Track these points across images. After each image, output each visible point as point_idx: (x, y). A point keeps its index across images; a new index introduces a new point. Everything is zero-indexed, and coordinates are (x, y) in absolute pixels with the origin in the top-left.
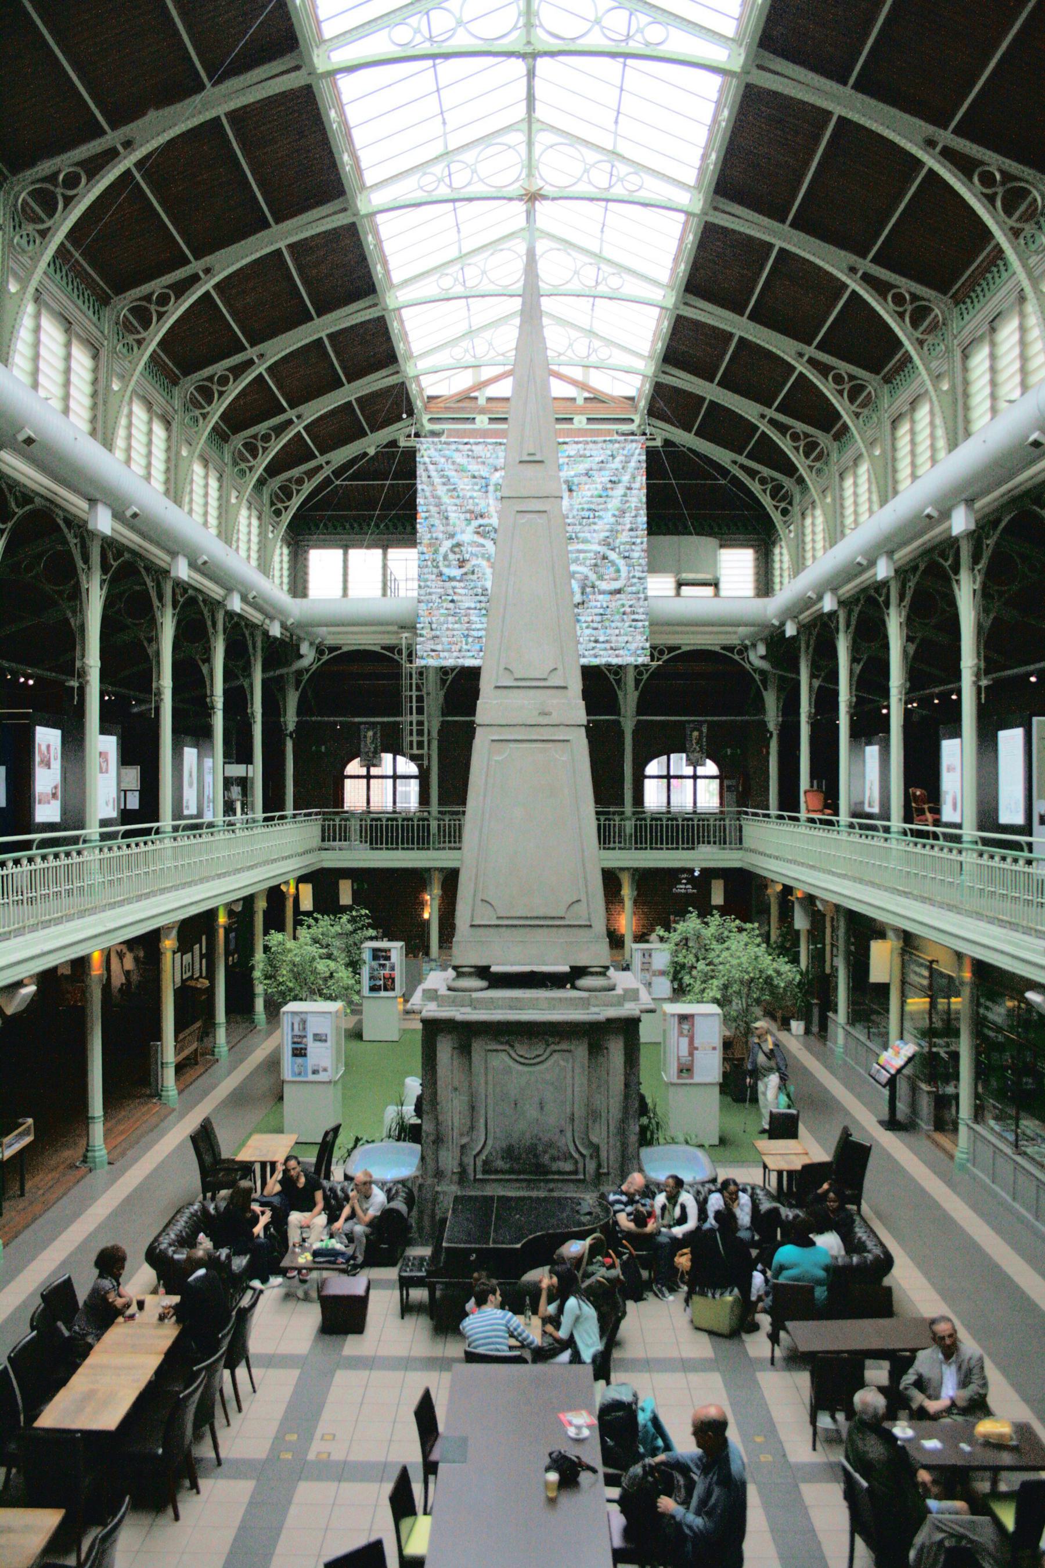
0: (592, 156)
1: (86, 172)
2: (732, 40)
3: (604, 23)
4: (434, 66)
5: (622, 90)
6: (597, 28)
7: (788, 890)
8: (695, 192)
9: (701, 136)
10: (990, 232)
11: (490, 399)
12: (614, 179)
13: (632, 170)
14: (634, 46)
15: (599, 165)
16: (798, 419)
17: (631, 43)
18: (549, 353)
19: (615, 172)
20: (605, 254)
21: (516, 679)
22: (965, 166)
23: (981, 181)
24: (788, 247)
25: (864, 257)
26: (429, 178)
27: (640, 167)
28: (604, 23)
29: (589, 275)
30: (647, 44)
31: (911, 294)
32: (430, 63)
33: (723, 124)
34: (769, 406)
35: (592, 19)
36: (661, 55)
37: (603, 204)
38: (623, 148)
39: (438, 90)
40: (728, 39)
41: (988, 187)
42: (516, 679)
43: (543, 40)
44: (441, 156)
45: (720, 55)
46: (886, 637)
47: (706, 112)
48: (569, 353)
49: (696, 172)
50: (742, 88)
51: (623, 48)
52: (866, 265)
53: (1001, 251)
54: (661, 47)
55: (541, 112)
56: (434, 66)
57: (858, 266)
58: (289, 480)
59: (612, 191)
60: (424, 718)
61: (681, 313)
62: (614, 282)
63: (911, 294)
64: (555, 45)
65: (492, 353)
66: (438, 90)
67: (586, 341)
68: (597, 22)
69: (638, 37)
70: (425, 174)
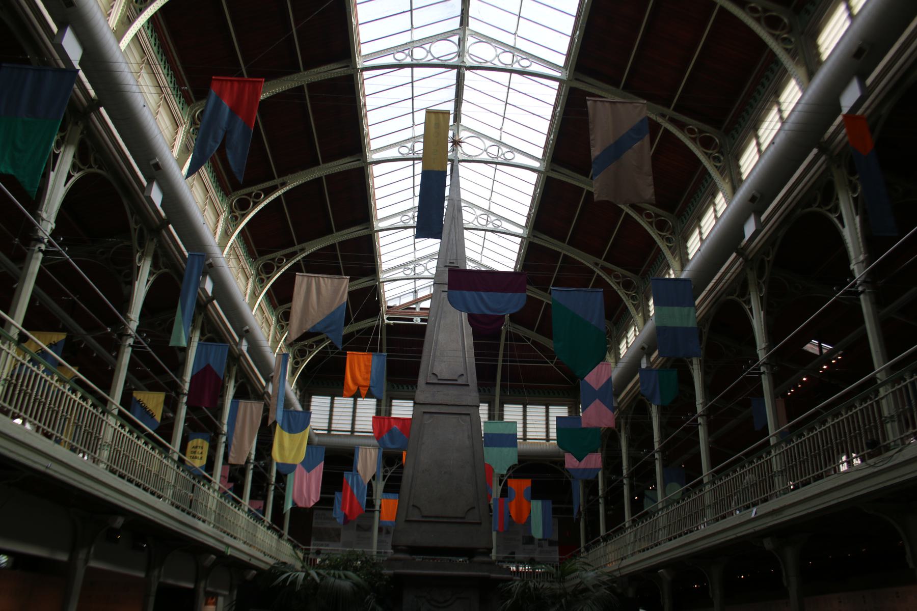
0: (479, 212)
1: (263, 192)
2: (562, 67)
3: (488, 151)
4: (413, 165)
5: (509, 88)
6: (485, 152)
8: (525, 229)
10: (655, 241)
11: (421, 309)
13: (496, 218)
14: (500, 160)
16: (618, 265)
17: (499, 159)
18: (464, 222)
20: (517, 46)
23: (614, 277)
24: (567, 253)
25: (669, 107)
26: (404, 218)
28: (488, 151)
30: (506, 159)
31: (655, 214)
32: (413, 280)
40: (561, 67)
41: (692, 134)
43: (469, 61)
44: (411, 138)
45: (536, 165)
46: (656, 479)
48: (475, 222)
49: (530, 198)
50: (545, 178)
52: (601, 262)
53: (660, 250)
54: (527, 69)
56: (413, 165)
57: (598, 262)
58: (273, 259)
62: (525, 63)
63: (655, 214)
64: (466, 158)
65: (430, 57)
68: (486, 150)
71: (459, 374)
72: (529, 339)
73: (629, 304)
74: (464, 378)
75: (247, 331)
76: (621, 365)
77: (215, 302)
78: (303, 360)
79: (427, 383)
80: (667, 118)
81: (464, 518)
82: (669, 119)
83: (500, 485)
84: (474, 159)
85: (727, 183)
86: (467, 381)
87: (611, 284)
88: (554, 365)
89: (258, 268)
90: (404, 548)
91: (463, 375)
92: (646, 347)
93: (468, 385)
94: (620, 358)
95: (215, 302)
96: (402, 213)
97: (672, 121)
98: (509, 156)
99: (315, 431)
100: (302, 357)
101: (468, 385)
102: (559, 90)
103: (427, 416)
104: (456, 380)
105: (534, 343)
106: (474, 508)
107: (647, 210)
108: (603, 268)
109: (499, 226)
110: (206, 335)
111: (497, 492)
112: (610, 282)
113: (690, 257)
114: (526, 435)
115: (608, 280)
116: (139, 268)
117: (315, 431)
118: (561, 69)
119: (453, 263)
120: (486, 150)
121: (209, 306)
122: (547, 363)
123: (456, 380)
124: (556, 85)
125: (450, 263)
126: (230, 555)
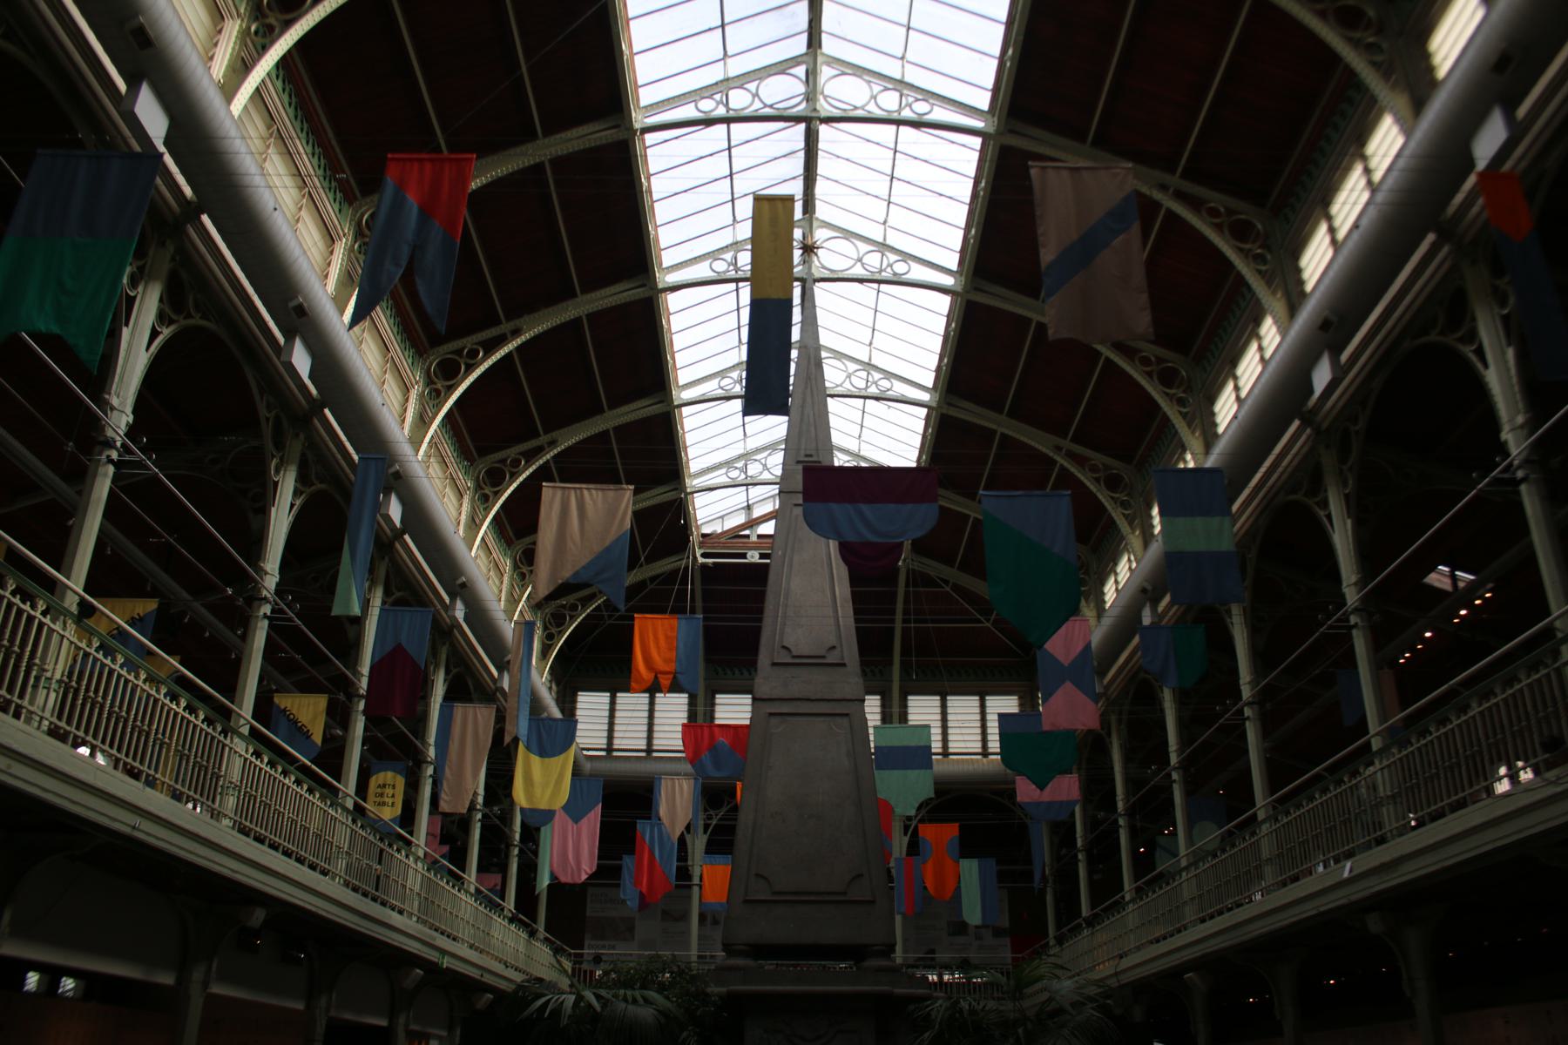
0: (852, 367)
3: (864, 261)
7: (162, 792)
9: (936, 344)
11: (760, 536)
12: (869, 384)
15: (858, 374)
17: (883, 274)
19: (870, 379)
21: (794, 657)
22: (1195, 204)
27: (889, 375)
29: (874, 260)
30: (895, 274)
32: (733, 286)
33: (929, 437)
34: (1065, 436)
35: (856, 258)
36: (888, 397)
37: (875, 286)
38: (914, 76)
39: (723, 26)
40: (982, 111)
42: (794, 657)
43: (825, 108)
45: (925, 397)
47: (940, 325)
51: (877, 277)
52: (1067, 444)
54: (903, 277)
55: (829, 46)
56: (737, 290)
59: (869, 390)
60: (396, 800)
61: (945, 411)
62: (921, 107)
64: (826, 274)
66: (731, 175)
67: (864, 374)
68: (860, 260)
69: (889, 270)
70: (723, 378)
71: (831, 645)
72: (946, 582)
73: (1117, 515)
74: (836, 652)
75: (464, 585)
76: (1107, 621)
77: (407, 537)
78: (560, 632)
79: (774, 664)
80: (1171, 191)
81: (845, 893)
82: (1066, 454)
83: (906, 834)
84: (841, 275)
85: (1197, 438)
86: (842, 658)
87: (1085, 481)
88: (993, 624)
89: (478, 477)
90: (742, 947)
91: (834, 647)
92: (1149, 588)
93: (844, 665)
94: (1104, 608)
95: (407, 537)
96: (722, 374)
97: (1180, 196)
98: (900, 268)
99: (585, 752)
100: (558, 626)
101: (844, 665)
102: (983, 151)
103: (774, 720)
104: (823, 657)
105: (956, 588)
106: (860, 876)
107: (1141, 351)
108: (1071, 455)
109: (888, 390)
110: (393, 594)
111: (901, 848)
112: (1082, 478)
113: (1221, 430)
114: (948, 748)
115: (1079, 475)
116: (276, 484)
117: (585, 752)
118: (985, 114)
119: (811, 456)
120: (860, 260)
121: (398, 546)
122: (979, 621)
123: (823, 657)
124: (977, 142)
125: (807, 456)
126: (447, 968)
